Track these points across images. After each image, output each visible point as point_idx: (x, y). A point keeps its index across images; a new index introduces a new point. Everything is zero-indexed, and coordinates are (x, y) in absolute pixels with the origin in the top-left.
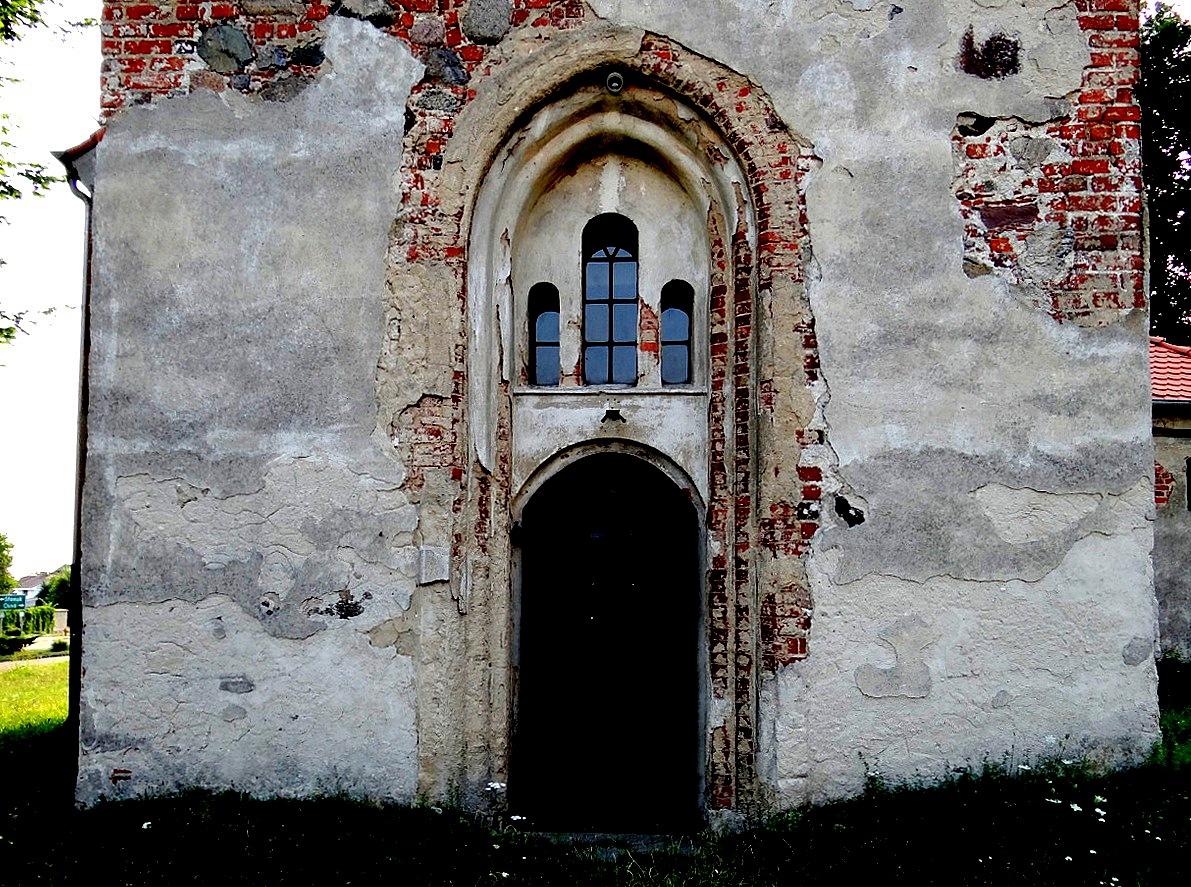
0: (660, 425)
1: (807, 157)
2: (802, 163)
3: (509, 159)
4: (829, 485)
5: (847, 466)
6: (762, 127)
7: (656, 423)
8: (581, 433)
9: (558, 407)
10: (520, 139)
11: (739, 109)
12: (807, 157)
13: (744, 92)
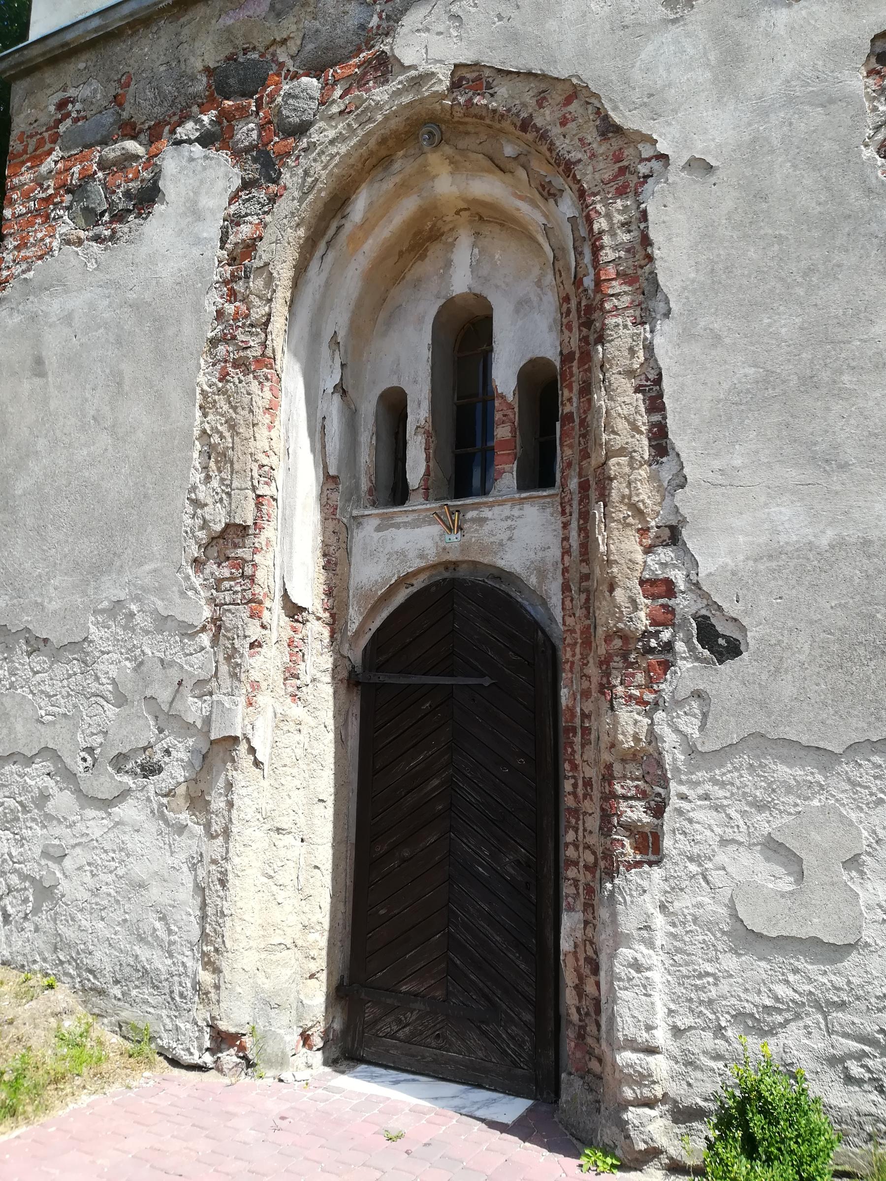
0: (510, 539)
1: (649, 160)
2: (643, 169)
3: (329, 252)
4: (685, 604)
5: (710, 574)
6: (592, 135)
7: (504, 536)
8: (421, 556)
9: (398, 528)
10: (339, 228)
11: (563, 124)
12: (649, 160)
13: (568, 101)
